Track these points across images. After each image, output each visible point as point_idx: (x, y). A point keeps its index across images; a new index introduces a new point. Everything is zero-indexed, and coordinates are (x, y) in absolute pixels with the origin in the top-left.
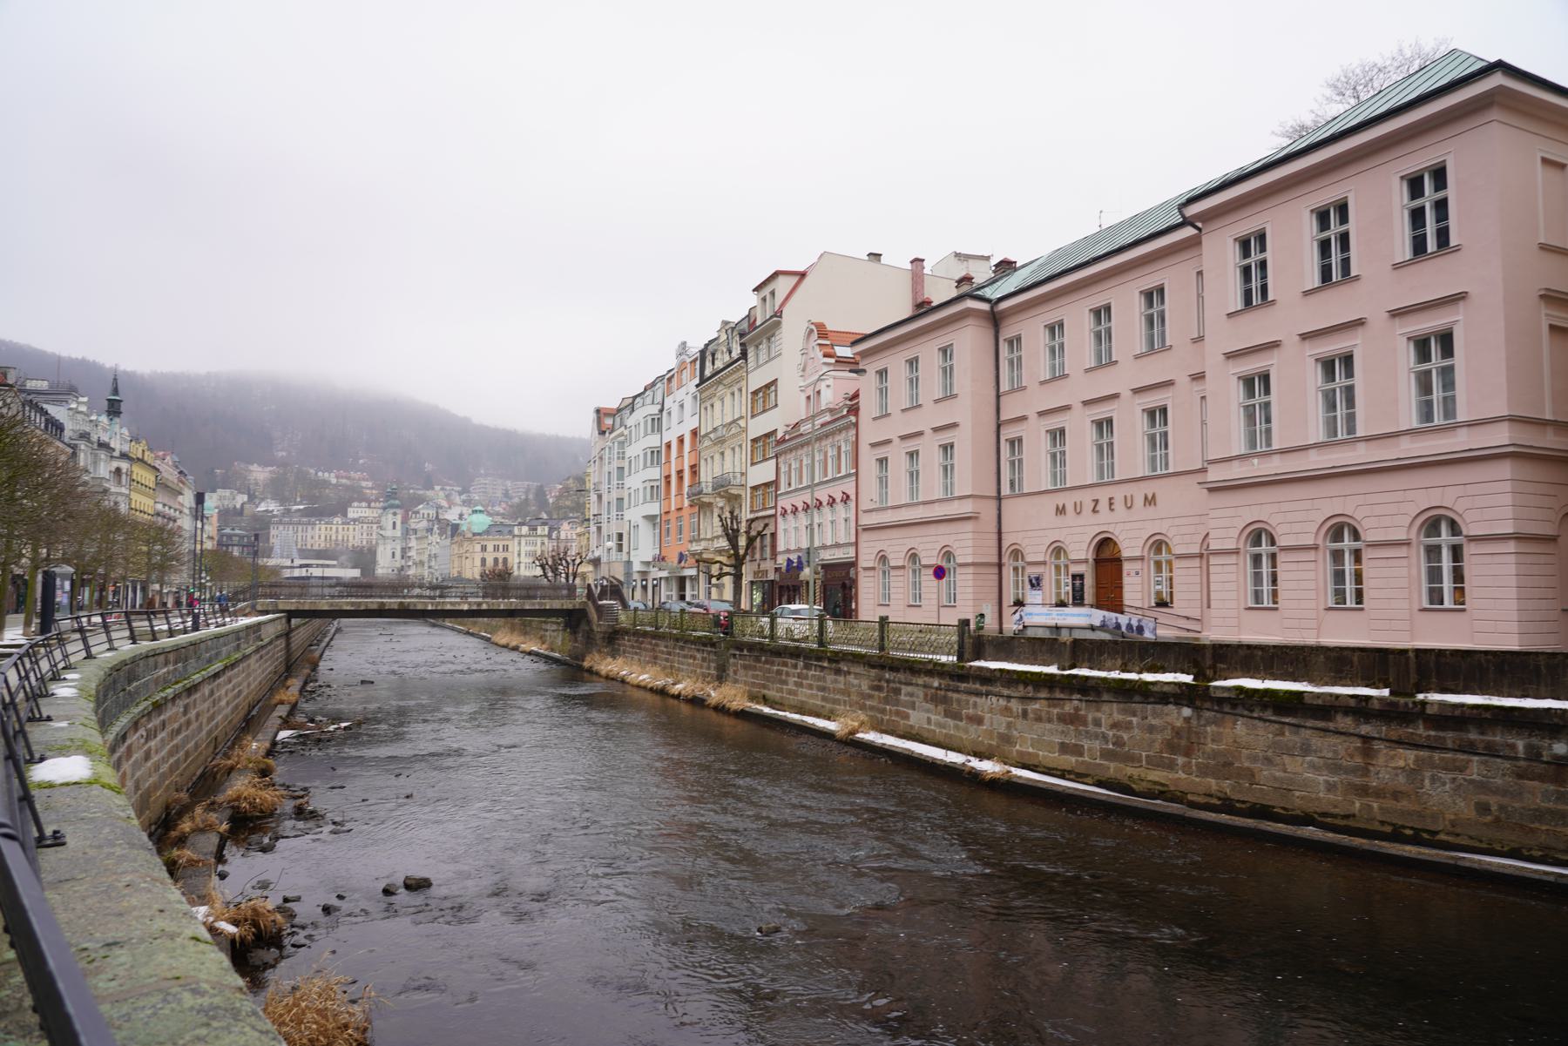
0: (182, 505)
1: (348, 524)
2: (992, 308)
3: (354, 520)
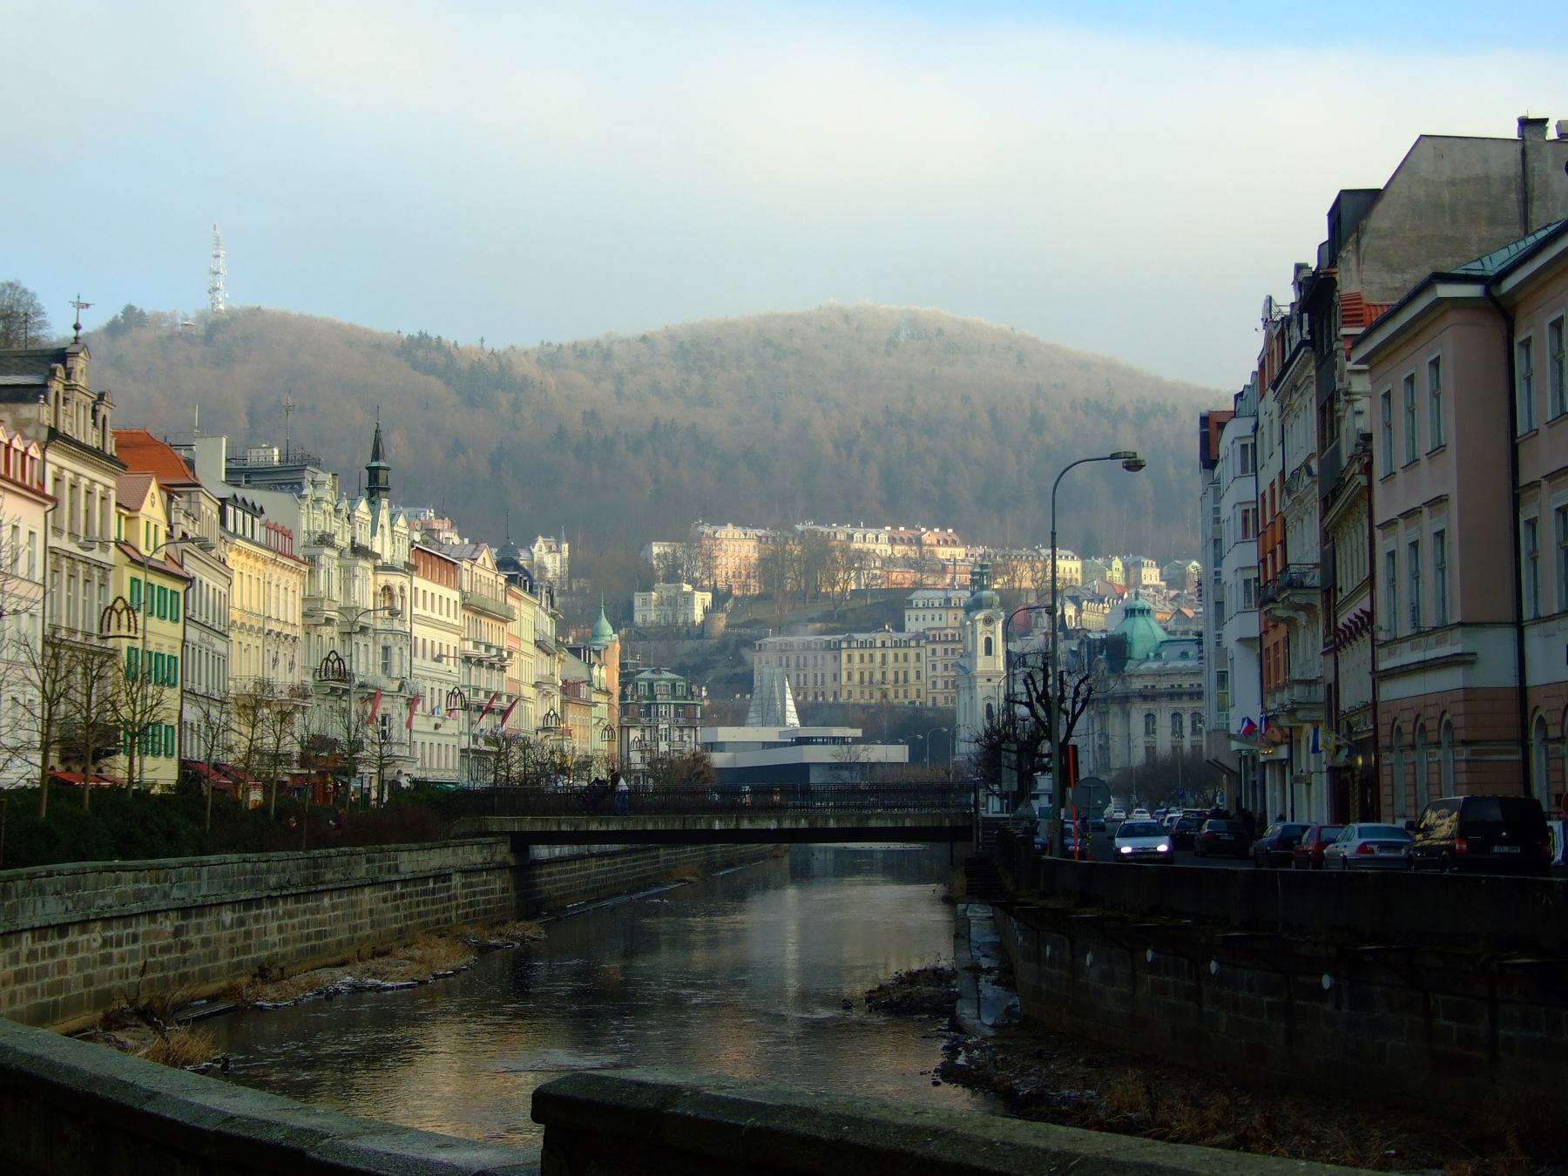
1: (907, 645)
2: (1487, 291)
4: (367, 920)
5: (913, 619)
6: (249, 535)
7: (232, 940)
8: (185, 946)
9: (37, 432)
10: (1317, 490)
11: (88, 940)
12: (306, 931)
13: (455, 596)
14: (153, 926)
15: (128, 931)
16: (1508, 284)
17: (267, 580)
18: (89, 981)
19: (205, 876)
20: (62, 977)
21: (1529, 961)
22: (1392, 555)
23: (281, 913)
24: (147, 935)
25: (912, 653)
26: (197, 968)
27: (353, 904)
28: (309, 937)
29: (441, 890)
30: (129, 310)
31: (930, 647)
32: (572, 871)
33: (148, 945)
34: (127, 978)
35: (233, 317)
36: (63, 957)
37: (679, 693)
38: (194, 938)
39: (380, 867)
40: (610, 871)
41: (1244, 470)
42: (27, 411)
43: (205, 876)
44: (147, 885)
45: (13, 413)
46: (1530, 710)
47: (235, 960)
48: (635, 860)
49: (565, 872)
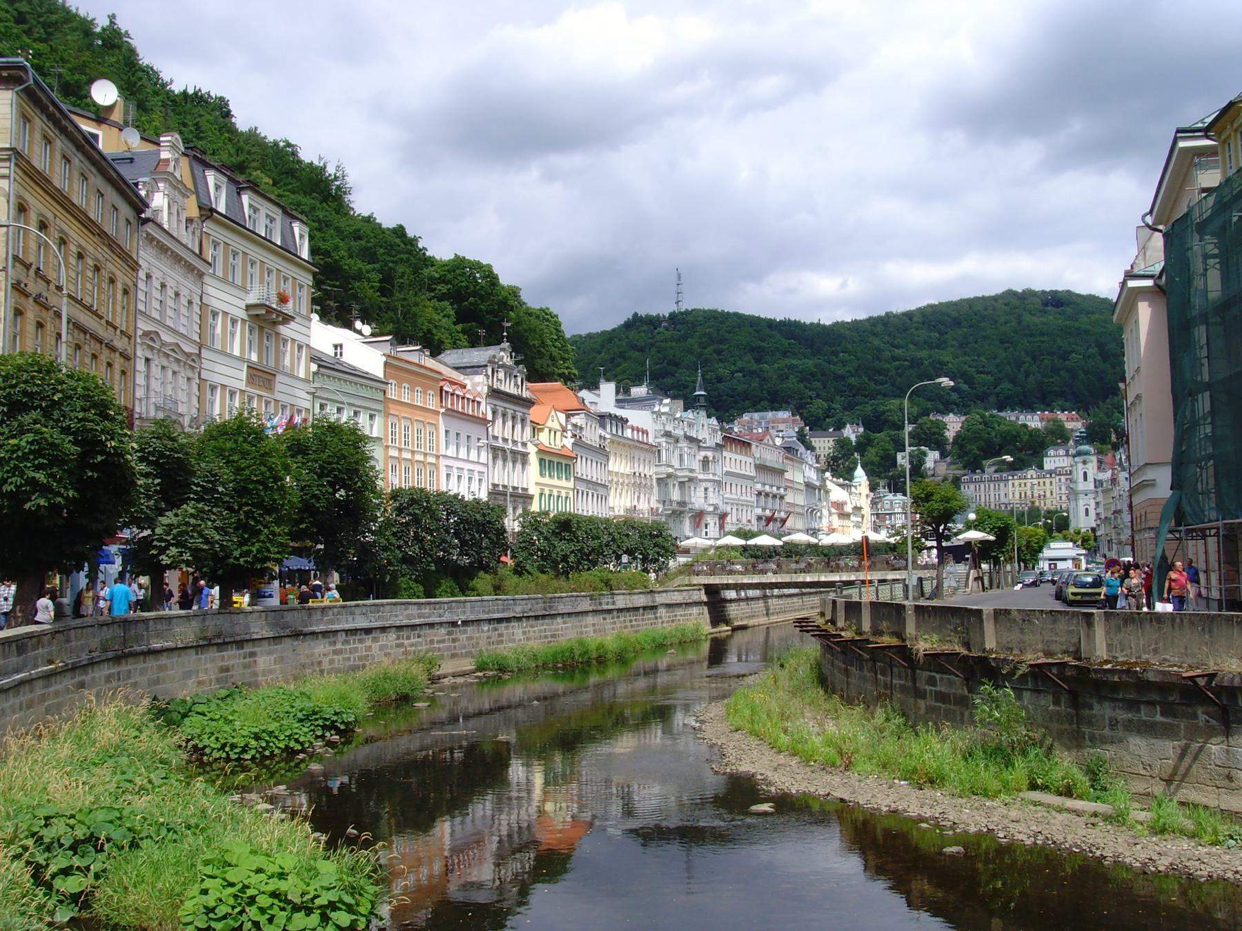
0: (692, 471)
3: (1051, 472)
25: (1047, 481)
30: (636, 314)
31: (1057, 478)
35: (687, 313)
45: (471, 380)
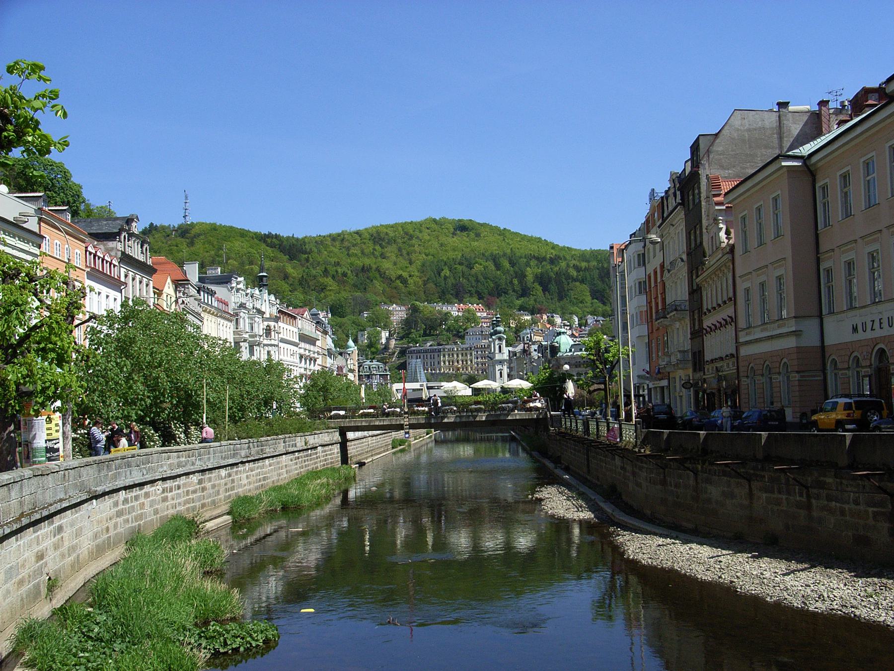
2: (805, 163)
4: (284, 470)
5: (468, 339)
6: (210, 303)
7: (226, 484)
8: (204, 489)
9: (116, 253)
10: (686, 268)
11: (155, 490)
12: (259, 477)
13: (296, 330)
14: (187, 480)
15: (175, 483)
16: (814, 159)
17: (219, 322)
18: (156, 512)
19: (212, 452)
20: (142, 511)
21: (865, 473)
22: (747, 291)
23: (247, 469)
24: (184, 485)
26: (210, 500)
27: (278, 463)
28: (260, 481)
29: (314, 454)
30: (152, 224)
32: (362, 443)
33: (185, 490)
34: (176, 508)
36: (142, 500)
37: (381, 370)
38: (208, 485)
39: (289, 445)
40: (376, 442)
41: (639, 265)
42: (111, 244)
43: (212, 452)
44: (184, 459)
46: (827, 355)
47: (228, 494)
48: (384, 437)
49: (360, 444)
